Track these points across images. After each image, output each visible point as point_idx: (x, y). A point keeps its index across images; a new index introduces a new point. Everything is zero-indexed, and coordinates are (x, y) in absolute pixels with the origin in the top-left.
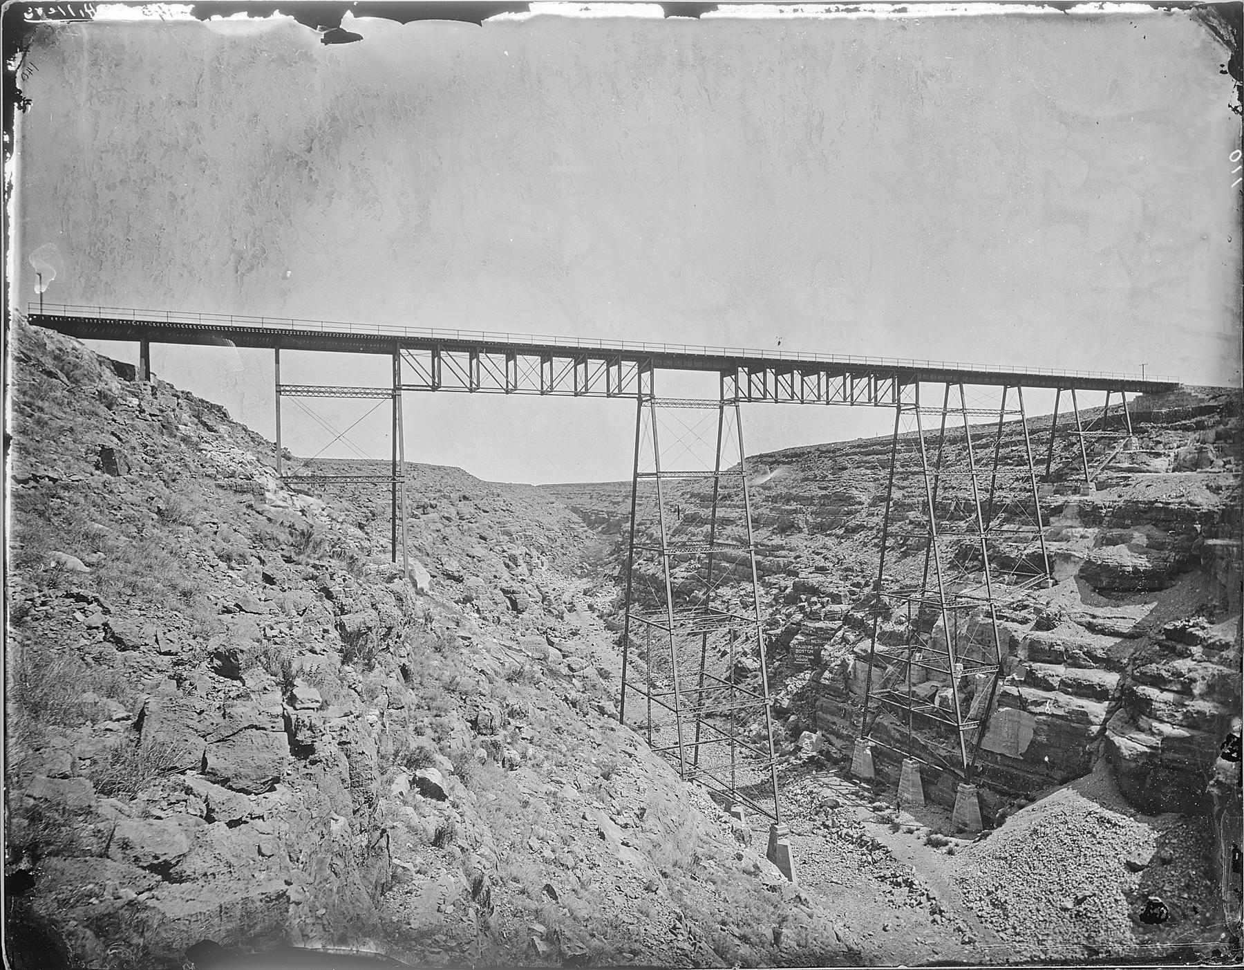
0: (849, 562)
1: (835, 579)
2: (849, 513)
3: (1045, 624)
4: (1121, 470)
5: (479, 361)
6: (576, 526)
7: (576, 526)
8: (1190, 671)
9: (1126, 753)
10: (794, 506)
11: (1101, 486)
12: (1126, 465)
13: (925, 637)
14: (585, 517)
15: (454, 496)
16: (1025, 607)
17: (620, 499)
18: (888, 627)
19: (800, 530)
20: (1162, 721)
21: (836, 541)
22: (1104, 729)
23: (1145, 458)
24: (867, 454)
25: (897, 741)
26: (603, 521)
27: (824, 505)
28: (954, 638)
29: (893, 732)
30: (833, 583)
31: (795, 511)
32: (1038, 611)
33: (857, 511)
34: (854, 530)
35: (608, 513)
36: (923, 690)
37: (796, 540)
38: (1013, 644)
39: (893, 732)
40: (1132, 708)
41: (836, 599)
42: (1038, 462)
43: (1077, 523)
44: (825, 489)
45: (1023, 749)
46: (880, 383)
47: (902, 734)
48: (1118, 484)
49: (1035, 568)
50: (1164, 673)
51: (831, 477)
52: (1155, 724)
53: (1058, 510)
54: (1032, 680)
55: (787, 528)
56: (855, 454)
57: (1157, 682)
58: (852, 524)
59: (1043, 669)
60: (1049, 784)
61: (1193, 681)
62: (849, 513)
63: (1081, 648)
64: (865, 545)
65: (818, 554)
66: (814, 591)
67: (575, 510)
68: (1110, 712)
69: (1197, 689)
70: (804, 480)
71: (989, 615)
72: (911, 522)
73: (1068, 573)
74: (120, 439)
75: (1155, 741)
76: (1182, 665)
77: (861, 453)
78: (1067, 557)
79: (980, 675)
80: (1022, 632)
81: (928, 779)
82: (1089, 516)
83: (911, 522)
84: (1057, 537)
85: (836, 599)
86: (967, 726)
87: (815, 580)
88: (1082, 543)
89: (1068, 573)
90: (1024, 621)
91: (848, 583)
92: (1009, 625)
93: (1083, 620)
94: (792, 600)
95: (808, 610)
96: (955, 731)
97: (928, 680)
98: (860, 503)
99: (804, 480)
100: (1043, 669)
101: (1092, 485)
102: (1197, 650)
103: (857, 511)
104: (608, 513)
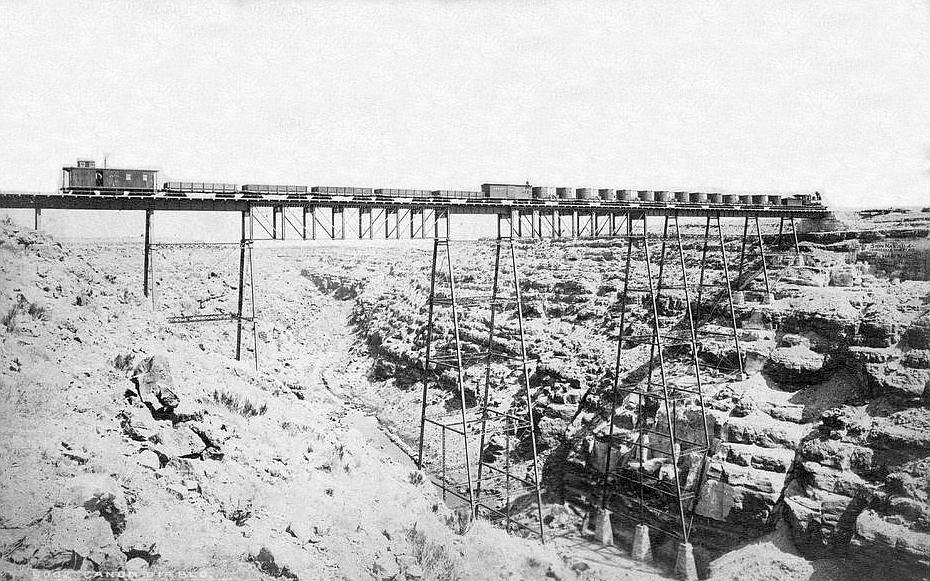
0: (585, 349)
1: (573, 364)
2: (581, 301)
3: (739, 412)
4: (790, 282)
5: (284, 218)
6: (312, 294)
7: (312, 294)
8: (840, 450)
9: (798, 515)
10: (532, 292)
11: (779, 296)
12: (795, 279)
13: (649, 421)
14: (317, 281)
15: (205, 273)
16: (725, 397)
17: (352, 264)
18: (619, 411)
19: (538, 315)
20: (821, 489)
21: (571, 326)
22: (782, 496)
23: (808, 273)
24: (593, 246)
25: (630, 509)
26: (333, 286)
27: (559, 292)
28: (675, 421)
29: (627, 502)
30: (571, 369)
31: (534, 298)
32: (735, 401)
33: (587, 300)
34: (586, 318)
35: (341, 278)
36: (649, 465)
37: (535, 325)
38: (717, 428)
39: (627, 502)
40: (801, 479)
41: (575, 384)
42: (732, 268)
43: (761, 327)
44: (560, 277)
45: (726, 514)
46: (599, 218)
47: (634, 504)
48: (790, 296)
49: (731, 364)
50: (822, 451)
51: (563, 267)
52: (817, 491)
53: (747, 316)
54: (733, 458)
55: (530, 312)
56: (582, 245)
57: (818, 458)
58: (583, 312)
59: (739, 449)
60: (744, 539)
61: (842, 458)
62: (581, 301)
63: (765, 431)
64: (596, 332)
65: (555, 338)
66: (556, 376)
67: (304, 273)
68: (787, 482)
69: (845, 464)
70: (540, 268)
71: (699, 403)
72: (633, 315)
73: (755, 369)
74: (622, 567)
75: (817, 505)
76: (833, 444)
77: (587, 245)
78: (754, 356)
79: (694, 454)
80: (723, 418)
81: (656, 540)
82: (766, 321)
83: (633, 315)
84: (748, 338)
85: (575, 384)
86: (684, 497)
87: (555, 364)
88: (764, 341)
89: (755, 369)
90: (725, 409)
91: (584, 369)
92: (716, 413)
93: (766, 408)
94: (535, 382)
95: (553, 394)
96: (676, 500)
97: (653, 457)
98: (590, 293)
99: (540, 268)
100: (739, 449)
101: (772, 296)
102: (843, 433)
103: (587, 300)
104: (341, 278)
